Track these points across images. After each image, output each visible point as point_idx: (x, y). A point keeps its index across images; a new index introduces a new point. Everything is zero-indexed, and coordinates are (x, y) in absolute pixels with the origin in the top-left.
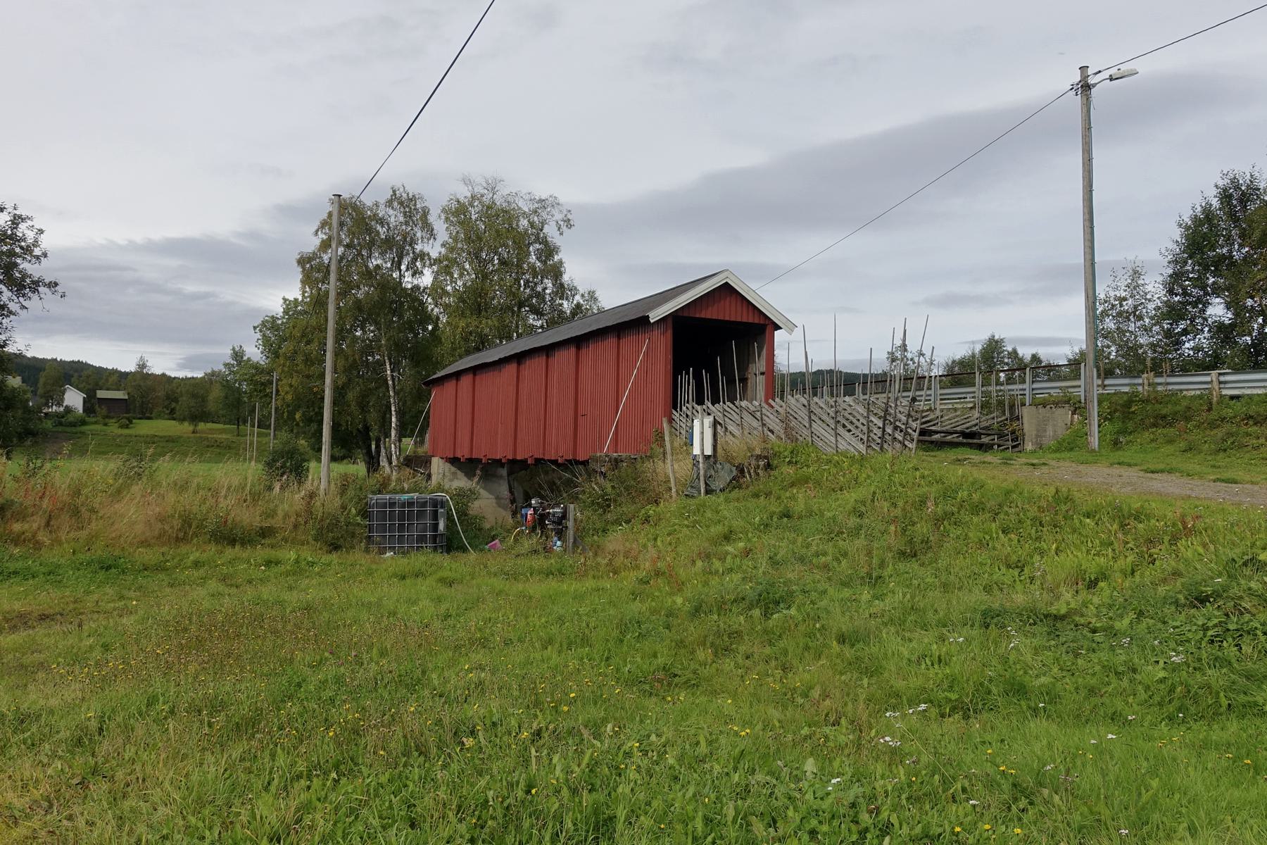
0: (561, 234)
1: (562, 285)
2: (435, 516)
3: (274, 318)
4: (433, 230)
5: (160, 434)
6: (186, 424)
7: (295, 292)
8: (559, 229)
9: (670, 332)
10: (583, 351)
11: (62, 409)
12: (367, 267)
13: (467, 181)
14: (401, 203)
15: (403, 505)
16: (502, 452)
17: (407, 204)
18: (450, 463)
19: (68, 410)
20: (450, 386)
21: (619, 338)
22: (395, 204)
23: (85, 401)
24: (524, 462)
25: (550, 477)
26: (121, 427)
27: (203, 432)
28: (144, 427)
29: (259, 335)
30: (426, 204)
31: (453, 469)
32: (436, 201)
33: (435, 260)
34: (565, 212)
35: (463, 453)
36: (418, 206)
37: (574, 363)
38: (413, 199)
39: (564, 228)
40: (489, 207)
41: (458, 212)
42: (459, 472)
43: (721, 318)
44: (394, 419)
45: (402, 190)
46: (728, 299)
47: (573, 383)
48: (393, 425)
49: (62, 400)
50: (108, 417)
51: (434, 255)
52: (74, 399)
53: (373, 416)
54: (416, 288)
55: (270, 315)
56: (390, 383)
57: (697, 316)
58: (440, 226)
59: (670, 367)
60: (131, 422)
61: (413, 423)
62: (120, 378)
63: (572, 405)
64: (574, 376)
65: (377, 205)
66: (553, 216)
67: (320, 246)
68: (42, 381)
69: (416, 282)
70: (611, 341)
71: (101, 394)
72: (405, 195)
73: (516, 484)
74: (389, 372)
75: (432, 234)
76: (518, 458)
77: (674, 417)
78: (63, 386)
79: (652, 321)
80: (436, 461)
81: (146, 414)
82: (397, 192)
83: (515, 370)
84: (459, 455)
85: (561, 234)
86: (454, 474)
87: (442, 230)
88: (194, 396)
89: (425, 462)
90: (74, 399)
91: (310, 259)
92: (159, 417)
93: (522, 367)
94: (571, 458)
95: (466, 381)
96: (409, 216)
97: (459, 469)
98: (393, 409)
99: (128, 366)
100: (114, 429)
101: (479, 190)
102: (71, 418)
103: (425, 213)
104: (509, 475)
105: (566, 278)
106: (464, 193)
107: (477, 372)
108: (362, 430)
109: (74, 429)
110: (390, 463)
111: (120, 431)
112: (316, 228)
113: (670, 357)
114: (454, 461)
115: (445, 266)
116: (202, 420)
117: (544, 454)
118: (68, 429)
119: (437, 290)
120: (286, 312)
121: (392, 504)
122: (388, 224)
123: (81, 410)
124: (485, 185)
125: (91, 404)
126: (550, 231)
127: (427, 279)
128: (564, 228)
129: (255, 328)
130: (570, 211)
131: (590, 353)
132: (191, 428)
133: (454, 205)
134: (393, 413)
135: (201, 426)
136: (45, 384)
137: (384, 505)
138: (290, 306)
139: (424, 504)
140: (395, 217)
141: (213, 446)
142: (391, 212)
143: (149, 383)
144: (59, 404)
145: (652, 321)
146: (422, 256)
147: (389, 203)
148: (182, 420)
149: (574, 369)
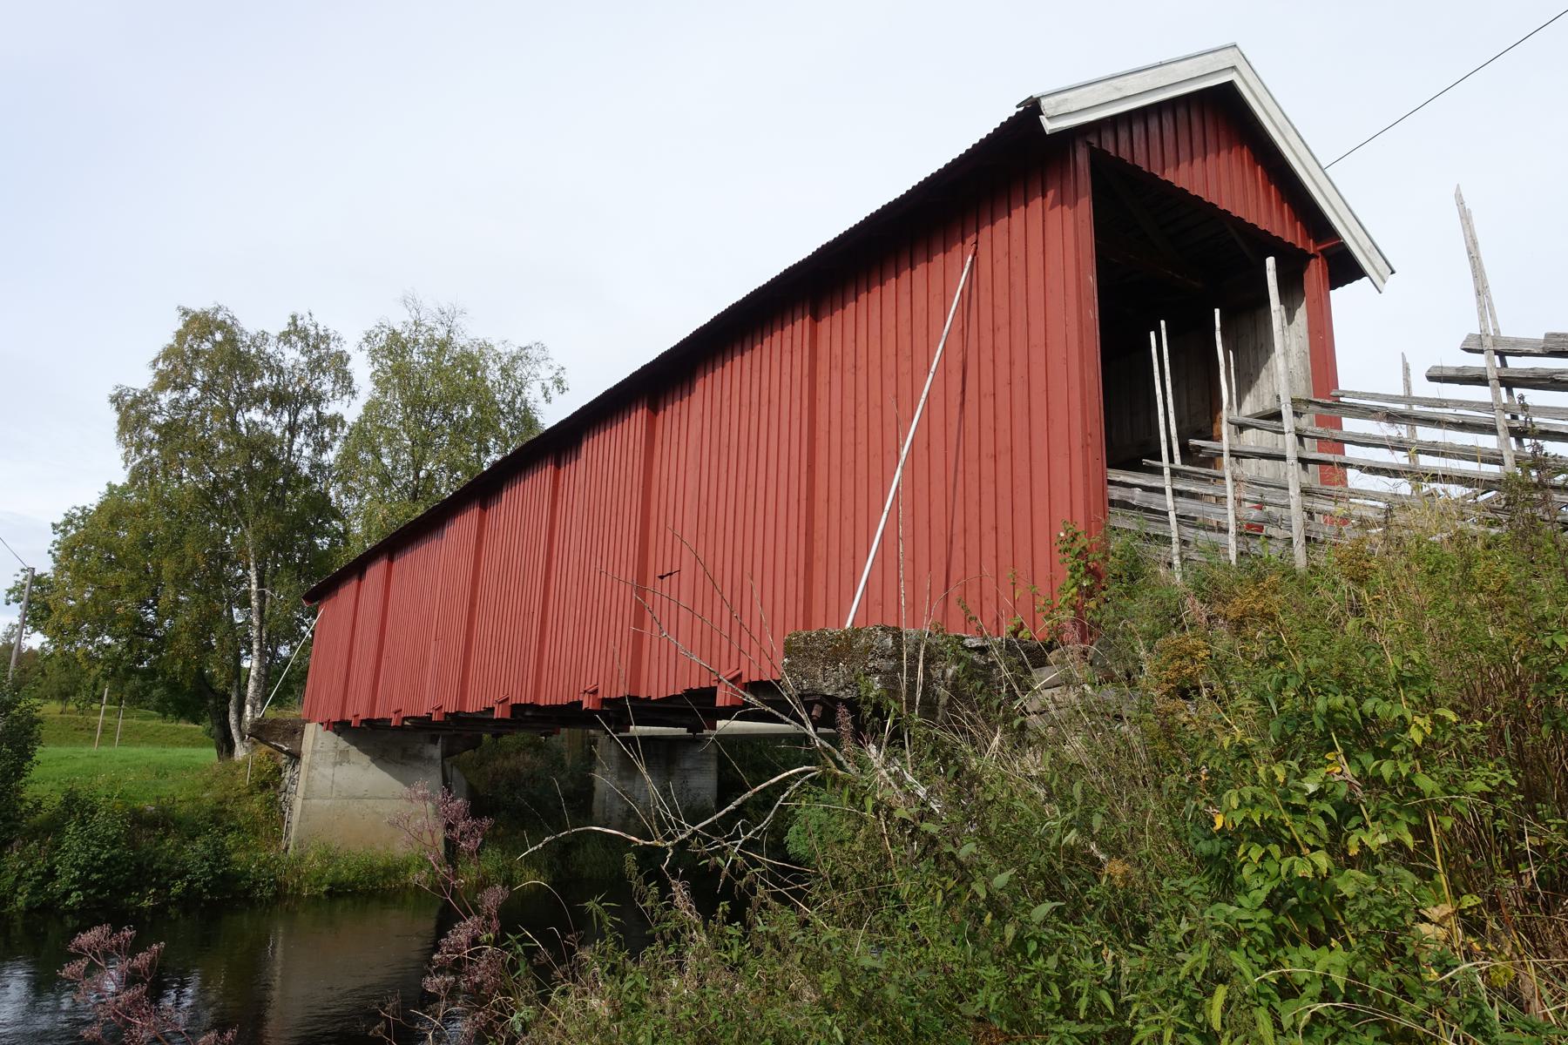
0: (549, 401)
4: (351, 383)
8: (545, 396)
9: (1085, 205)
12: (234, 423)
16: (433, 700)
18: (335, 731)
20: (347, 592)
25: (513, 762)
30: (345, 348)
35: (358, 710)
38: (324, 338)
39: (554, 393)
41: (393, 349)
42: (353, 749)
45: (307, 319)
57: (1169, 176)
58: (362, 370)
63: (633, 550)
64: (638, 478)
73: (455, 773)
80: (311, 730)
82: (299, 323)
83: (475, 520)
84: (349, 716)
87: (362, 370)
89: (294, 731)
91: (137, 401)
94: (623, 691)
95: (376, 572)
96: (316, 366)
97: (355, 744)
103: (341, 359)
104: (446, 755)
106: (399, 320)
107: (396, 556)
108: (1042, 956)
112: (156, 356)
114: (341, 727)
115: (362, 436)
124: (436, 311)
128: (554, 393)
130: (563, 369)
132: (59, 707)
140: (292, 356)
141: (82, 729)
142: (286, 349)
146: (335, 421)
147: (285, 337)
149: (639, 461)
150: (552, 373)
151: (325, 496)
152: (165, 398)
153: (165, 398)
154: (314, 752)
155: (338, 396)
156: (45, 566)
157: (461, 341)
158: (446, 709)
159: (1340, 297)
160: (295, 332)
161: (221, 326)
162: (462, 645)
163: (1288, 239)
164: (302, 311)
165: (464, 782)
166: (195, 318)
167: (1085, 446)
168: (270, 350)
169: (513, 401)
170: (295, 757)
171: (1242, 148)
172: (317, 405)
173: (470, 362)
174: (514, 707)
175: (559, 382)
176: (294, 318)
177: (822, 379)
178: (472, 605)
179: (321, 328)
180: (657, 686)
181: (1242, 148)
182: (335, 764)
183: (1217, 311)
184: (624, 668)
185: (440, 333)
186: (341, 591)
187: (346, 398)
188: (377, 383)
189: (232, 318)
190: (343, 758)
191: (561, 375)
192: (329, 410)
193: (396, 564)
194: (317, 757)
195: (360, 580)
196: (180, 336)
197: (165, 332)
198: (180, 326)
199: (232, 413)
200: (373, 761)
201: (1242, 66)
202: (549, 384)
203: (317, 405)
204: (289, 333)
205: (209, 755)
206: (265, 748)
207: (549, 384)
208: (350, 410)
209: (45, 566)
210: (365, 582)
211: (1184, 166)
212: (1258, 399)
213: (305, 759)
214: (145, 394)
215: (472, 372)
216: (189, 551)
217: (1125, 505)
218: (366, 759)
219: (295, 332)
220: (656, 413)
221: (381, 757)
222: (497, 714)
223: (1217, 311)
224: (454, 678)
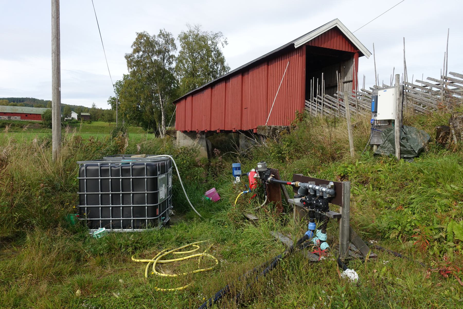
0: (224, 47)
1: (224, 67)
2: (154, 185)
3: (120, 82)
5: (99, 125)
6: (107, 123)
7: (126, 71)
9: (304, 57)
10: (246, 76)
11: (71, 118)
12: (151, 60)
13: (188, 25)
14: (164, 36)
15: (117, 173)
16: (205, 128)
17: (165, 35)
18: (184, 133)
19: (73, 118)
20: (183, 102)
21: (268, 65)
22: (161, 36)
23: (78, 116)
24: (215, 132)
25: (221, 138)
26: (88, 124)
27: (111, 125)
28: (95, 124)
29: (115, 88)
30: (173, 37)
31: (185, 135)
32: (175, 35)
33: (177, 58)
34: (225, 38)
35: (188, 129)
36: (170, 37)
37: (240, 84)
38: (168, 35)
39: (225, 45)
40: (197, 36)
41: (185, 38)
42: (187, 136)
43: (332, 48)
44: (163, 117)
45: (164, 30)
46: (335, 38)
47: (240, 93)
48: (163, 119)
49: (71, 116)
50: (84, 121)
51: (177, 56)
52: (74, 115)
53: (155, 116)
54: (170, 69)
55: (119, 80)
56: (161, 103)
57: (322, 46)
58: (178, 43)
59: (304, 75)
60: (91, 122)
61: (170, 120)
62: (87, 110)
63: (240, 103)
64: (240, 89)
65: (154, 36)
66: (220, 40)
67: (133, 52)
68: (64, 110)
69: (170, 66)
70: (263, 68)
71: (82, 114)
72: (165, 33)
73: (208, 141)
74: (160, 99)
75: (175, 48)
76: (212, 130)
77: (306, 104)
78: (71, 111)
79: (296, 47)
81: (96, 120)
82: (162, 32)
84: (187, 130)
85: (224, 47)
86: (185, 137)
87: (178, 43)
88: (109, 114)
89: (175, 133)
90: (74, 115)
91: (130, 57)
92: (100, 121)
93: (214, 90)
95: (189, 99)
96: (167, 42)
97: (187, 135)
98: (162, 113)
99: (90, 106)
100: (86, 124)
101: (193, 29)
102: (73, 121)
103: (173, 40)
104: (206, 137)
105: (225, 64)
106: (186, 30)
107: (194, 96)
109: (74, 124)
110: (162, 133)
111: (88, 125)
112: (132, 45)
113: (304, 69)
114: (185, 132)
115: (180, 60)
116: (111, 121)
117: (225, 128)
118: (73, 124)
119: (178, 69)
120: (124, 79)
121: (104, 172)
122: (159, 44)
123: (77, 119)
124: (194, 27)
125: (79, 117)
126: (219, 46)
127: (174, 65)
128: (225, 45)
129: (114, 85)
131: (249, 77)
132: (109, 124)
133: (183, 36)
134: (163, 115)
135: (112, 123)
136: (65, 111)
137: (95, 173)
138: (125, 77)
139: (140, 172)
140: (161, 41)
142: (160, 39)
143: (96, 111)
144: (70, 117)
145: (296, 47)
146: (172, 56)
147: (159, 36)
148: (106, 121)
149: (240, 86)
150: (224, 40)
151: (172, 75)
152: (136, 55)
153: (136, 55)
154: (179, 137)
155: (173, 50)
156: (114, 95)
157: (201, 34)
158: (207, 130)
159: (360, 59)
160: (162, 34)
161: (145, 36)
162: (210, 117)
163: (350, 51)
164: (162, 29)
165: (211, 143)
166: (140, 35)
167: (301, 97)
168: (156, 40)
169: (215, 48)
170: (176, 138)
171: (340, 35)
172: (168, 53)
173: (204, 39)
174: (220, 130)
175: (226, 42)
176: (161, 31)
177: (269, 77)
178: (211, 109)
179: (167, 33)
180: (245, 129)
181: (340, 35)
182: (184, 139)
183: (323, 73)
184: (240, 126)
185: (196, 32)
186: (181, 102)
187: (175, 50)
188: (182, 47)
189: (148, 34)
190: (185, 138)
191: (226, 40)
192: (171, 53)
193: (194, 97)
194: (180, 138)
195: (185, 100)
196: (137, 39)
197: (134, 38)
198: (137, 37)
199: (151, 58)
200: (191, 139)
201: (339, 23)
202: (223, 43)
203: (168, 53)
204: (160, 35)
205: (153, 136)
206: (168, 136)
207: (223, 43)
208: (176, 53)
209: (114, 95)
210: (187, 101)
211: (326, 43)
212: (347, 78)
213: (177, 138)
214: (131, 54)
215: (205, 42)
216: (146, 92)
217: (307, 106)
218: (190, 138)
219: (162, 34)
220: (243, 76)
221: (193, 138)
222: (218, 132)
223: (323, 73)
224: (209, 123)
